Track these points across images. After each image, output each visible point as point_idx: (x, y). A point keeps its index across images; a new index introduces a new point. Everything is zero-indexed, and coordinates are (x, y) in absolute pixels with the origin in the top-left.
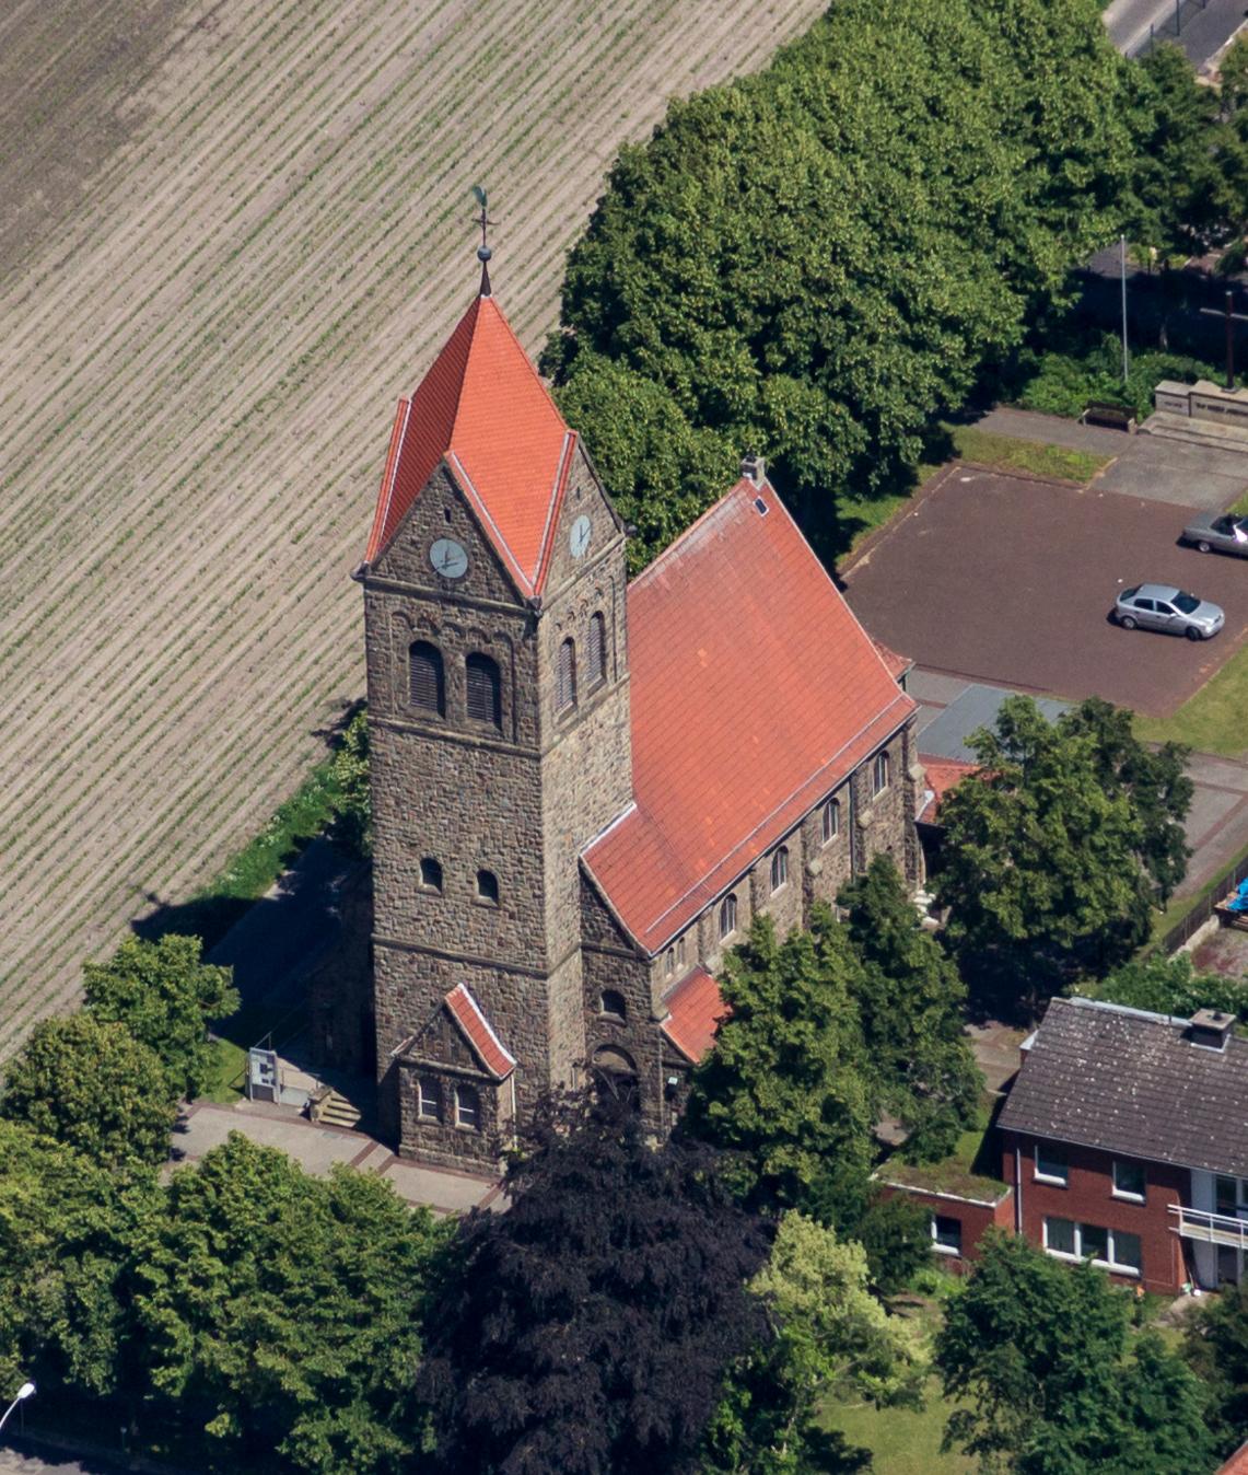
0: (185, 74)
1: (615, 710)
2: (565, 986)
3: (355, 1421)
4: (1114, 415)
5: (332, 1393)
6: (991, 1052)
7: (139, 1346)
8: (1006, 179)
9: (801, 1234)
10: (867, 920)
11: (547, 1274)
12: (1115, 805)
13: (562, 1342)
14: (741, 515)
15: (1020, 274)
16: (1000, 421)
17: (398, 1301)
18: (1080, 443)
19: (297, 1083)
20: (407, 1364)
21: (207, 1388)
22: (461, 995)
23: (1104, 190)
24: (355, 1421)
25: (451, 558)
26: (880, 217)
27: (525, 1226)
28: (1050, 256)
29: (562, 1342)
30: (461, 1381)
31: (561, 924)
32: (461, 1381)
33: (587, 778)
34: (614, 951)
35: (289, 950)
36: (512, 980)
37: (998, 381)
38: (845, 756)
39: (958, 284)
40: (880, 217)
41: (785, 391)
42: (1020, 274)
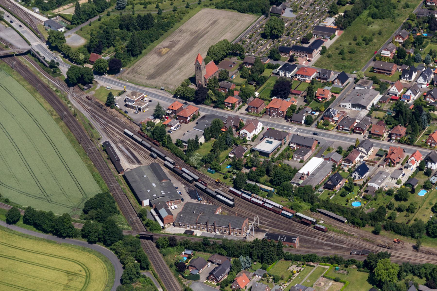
0: (197, 44)
1: (205, 70)
2: (203, 81)
3: (192, 98)
4: (230, 58)
5: (191, 97)
6: (220, 83)
7: (184, 95)
8: (225, 48)
9: (210, 90)
10: (215, 78)
11: (199, 92)
12: (226, 74)
13: (199, 95)
14: (212, 62)
15: (226, 52)
16: (226, 58)
17: (194, 93)
18: (229, 59)
19: (193, 84)
20: (194, 95)
21: (187, 96)
22: (199, 81)
23: (230, 49)
24: (192, 98)
25: (198, 64)
26: (219, 50)
27: (198, 90)
28: (227, 52)
29: (199, 95)
30: (412, 43)
31: (203, 78)
32: (412, 43)
33: (204, 72)
34: (205, 79)
35: (193, 80)
36: (201, 80)
37: (225, 57)
38: (215, 71)
39: (222, 53)
40: (219, 50)
41: (215, 57)
42: (226, 52)
